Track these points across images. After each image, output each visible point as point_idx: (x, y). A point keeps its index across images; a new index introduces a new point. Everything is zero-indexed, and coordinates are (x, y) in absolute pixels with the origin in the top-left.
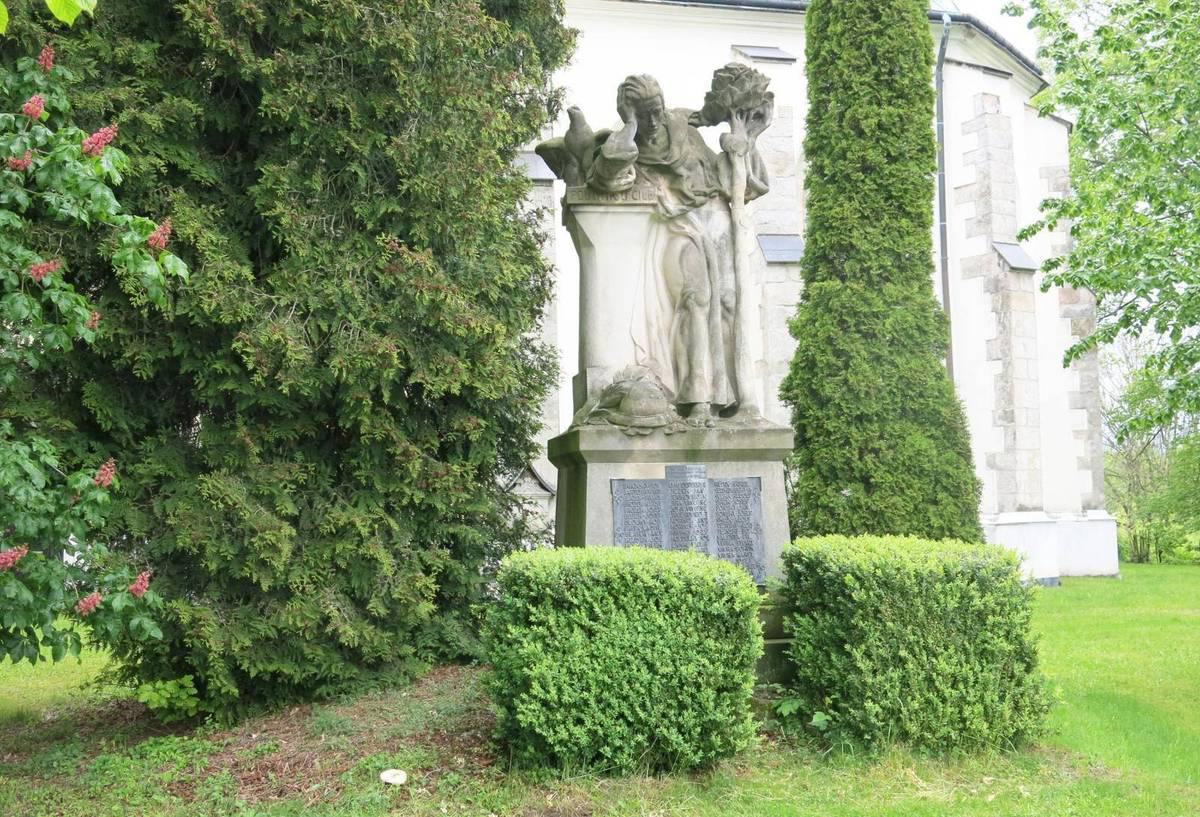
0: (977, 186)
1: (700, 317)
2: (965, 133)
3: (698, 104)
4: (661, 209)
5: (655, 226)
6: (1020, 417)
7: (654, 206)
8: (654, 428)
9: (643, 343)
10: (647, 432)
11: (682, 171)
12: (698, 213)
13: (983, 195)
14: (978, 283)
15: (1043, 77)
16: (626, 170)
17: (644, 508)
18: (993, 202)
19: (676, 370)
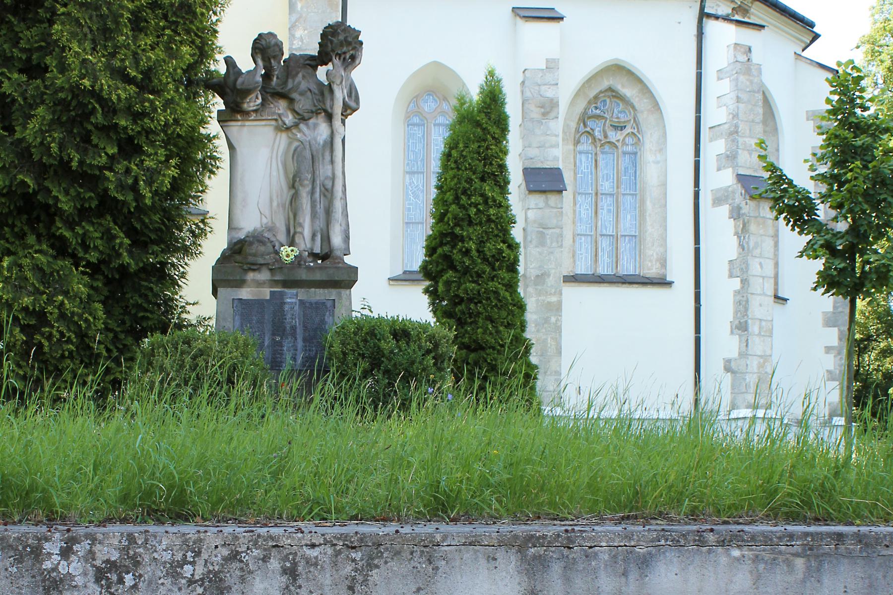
0: (726, 126)
1: (304, 193)
2: (719, 79)
3: (313, 49)
4: (280, 122)
5: (279, 134)
6: (754, 328)
7: (276, 120)
8: (261, 265)
9: (267, 212)
10: (255, 267)
11: (295, 95)
12: (307, 125)
13: (731, 134)
14: (725, 209)
15: (815, 29)
16: (253, 96)
17: (254, 317)
18: (741, 140)
19: (288, 231)
